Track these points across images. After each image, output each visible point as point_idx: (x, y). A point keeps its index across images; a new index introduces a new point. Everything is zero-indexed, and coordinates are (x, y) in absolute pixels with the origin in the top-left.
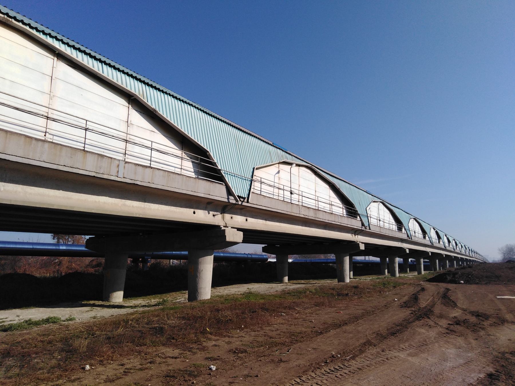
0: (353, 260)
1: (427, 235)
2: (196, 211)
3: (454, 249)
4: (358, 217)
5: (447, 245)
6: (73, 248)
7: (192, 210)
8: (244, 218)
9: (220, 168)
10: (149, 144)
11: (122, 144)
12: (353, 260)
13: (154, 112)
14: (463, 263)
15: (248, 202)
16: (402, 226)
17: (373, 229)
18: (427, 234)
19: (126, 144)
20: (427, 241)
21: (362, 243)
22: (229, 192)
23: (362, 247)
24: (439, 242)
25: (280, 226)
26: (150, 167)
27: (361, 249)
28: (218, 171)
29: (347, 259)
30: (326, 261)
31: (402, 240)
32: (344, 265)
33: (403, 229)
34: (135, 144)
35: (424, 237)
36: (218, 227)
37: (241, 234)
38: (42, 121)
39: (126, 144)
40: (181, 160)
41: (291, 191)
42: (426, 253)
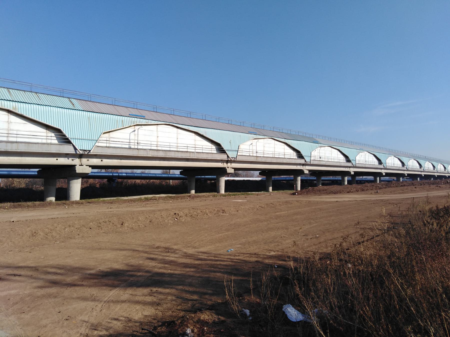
0: (381, 180)
2: (58, 158)
6: (98, 174)
7: (56, 158)
8: (101, 160)
9: (68, 137)
12: (381, 180)
15: (236, 159)
19: (73, 140)
21: (384, 173)
23: (384, 174)
25: (142, 162)
26: (285, 158)
27: (227, 172)
29: (378, 178)
30: (285, 179)
31: (421, 172)
32: (220, 183)
36: (302, 170)
39: (73, 140)
42: (445, 176)
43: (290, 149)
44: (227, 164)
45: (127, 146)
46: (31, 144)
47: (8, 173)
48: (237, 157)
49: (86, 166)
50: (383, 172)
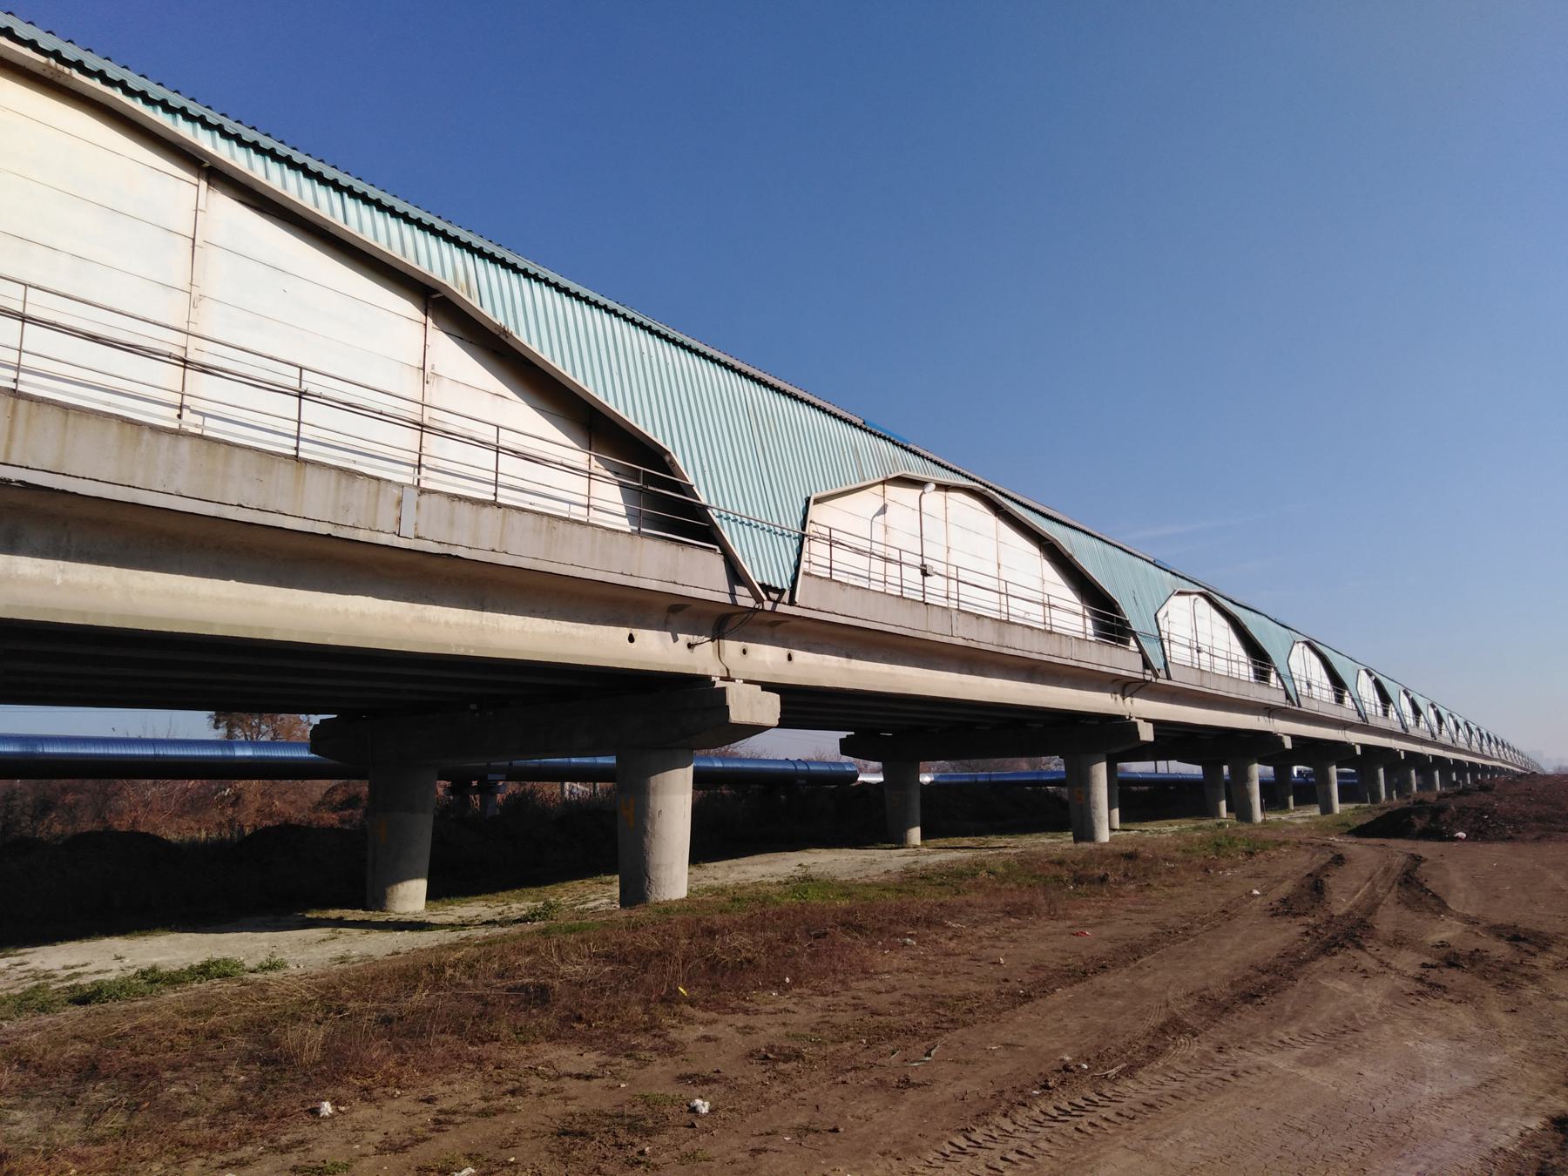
0: (1119, 775)
1: (1347, 694)
2: (637, 632)
3: (1433, 735)
4: (1132, 642)
5: (1410, 721)
6: (273, 754)
7: (626, 631)
8: (784, 652)
9: (704, 501)
10: (488, 434)
11: (410, 438)
12: (1119, 775)
13: (503, 337)
14: (1461, 776)
15: (792, 602)
16: (1270, 667)
17: (1180, 679)
18: (1347, 689)
20: (1347, 712)
21: (1146, 720)
22: (736, 574)
23: (1147, 733)
24: (1386, 713)
26: (495, 504)
27: (1142, 739)
28: (700, 511)
29: (1100, 771)
32: (1093, 789)
33: (1273, 676)
34: (447, 434)
35: (1340, 700)
36: (705, 680)
37: (774, 699)
38: (170, 374)
40: (587, 479)
41: (923, 565)
43: (1064, 584)
44: (1124, 699)
45: (1190, 665)
46: (237, 450)
47: (25, 750)
48: (794, 581)
49: (746, 682)
50: (1143, 711)
